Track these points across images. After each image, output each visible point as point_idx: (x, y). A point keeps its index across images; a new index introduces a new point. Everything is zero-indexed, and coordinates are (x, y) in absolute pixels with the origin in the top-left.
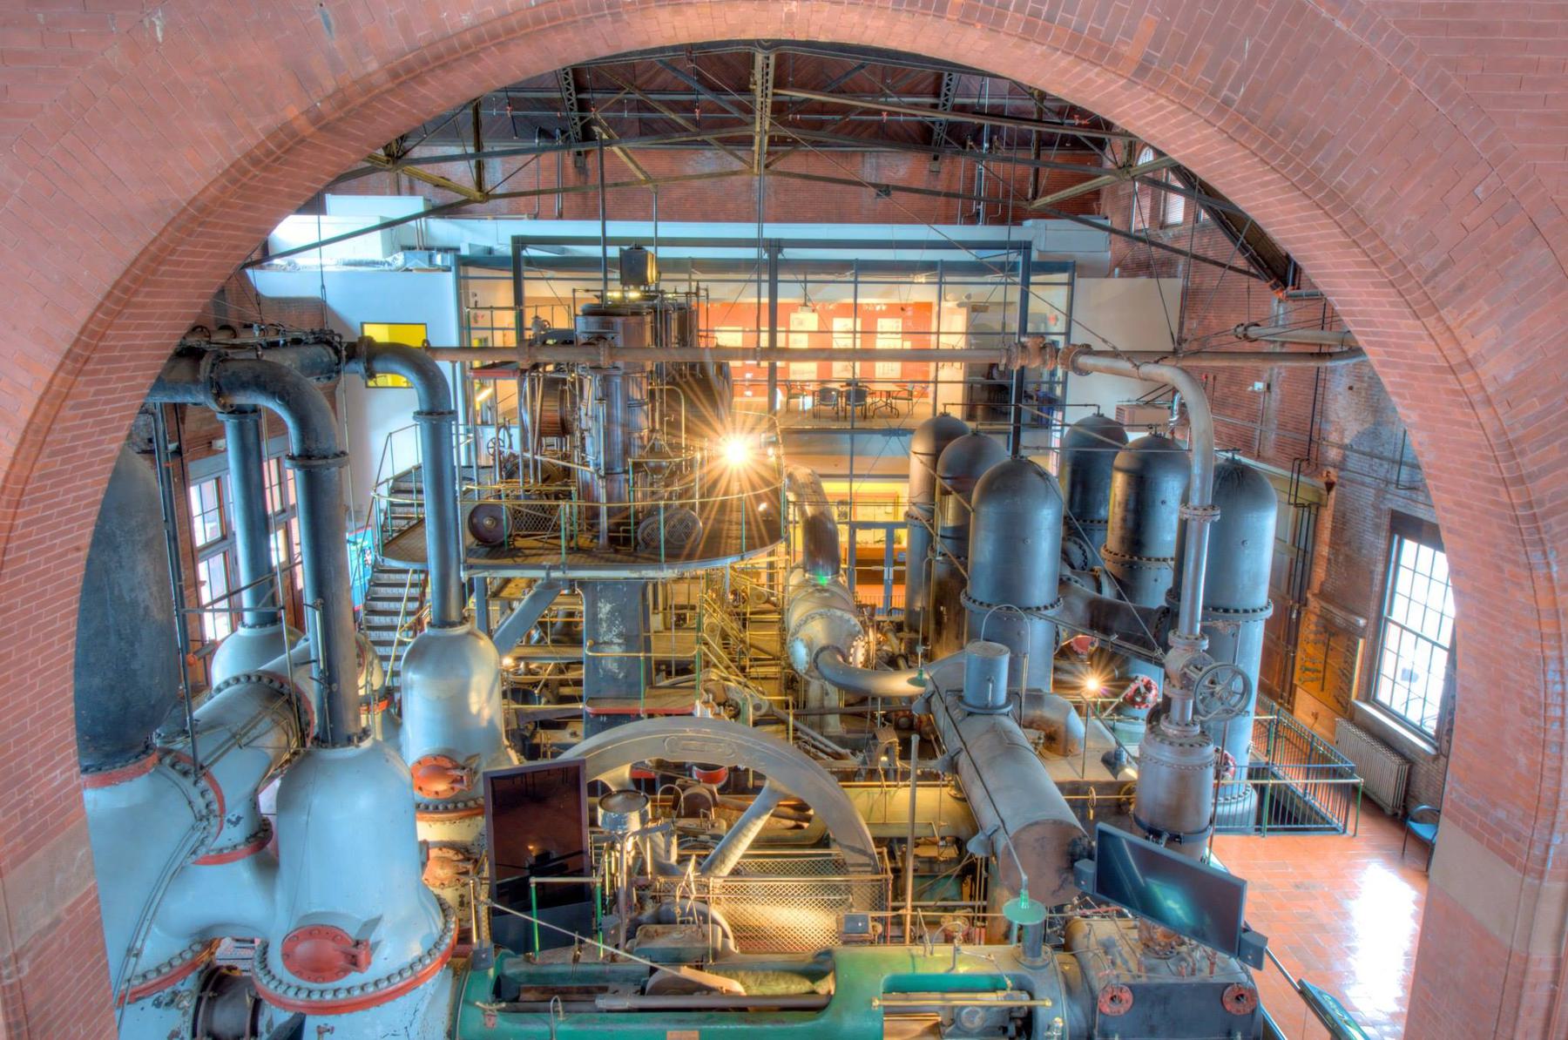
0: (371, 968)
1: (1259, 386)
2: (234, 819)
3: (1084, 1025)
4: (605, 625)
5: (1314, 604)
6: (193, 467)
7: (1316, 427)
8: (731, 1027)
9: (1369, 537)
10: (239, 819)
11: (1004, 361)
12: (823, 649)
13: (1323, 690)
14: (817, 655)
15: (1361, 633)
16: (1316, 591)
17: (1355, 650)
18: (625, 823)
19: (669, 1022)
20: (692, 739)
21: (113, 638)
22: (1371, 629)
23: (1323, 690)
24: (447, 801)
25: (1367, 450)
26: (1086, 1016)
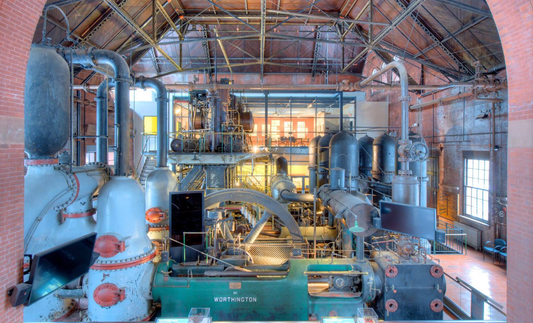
0: (124, 253)
1: (415, 125)
2: (83, 203)
3: (381, 283)
4: (213, 181)
5: (441, 188)
6: (87, 147)
7: (435, 132)
8: (253, 281)
9: (456, 161)
10: (85, 203)
11: (338, 88)
12: (283, 190)
13: (447, 215)
14: (281, 193)
15: (458, 192)
16: (441, 183)
17: (457, 199)
18: (217, 216)
19: (230, 280)
20: (240, 193)
21: (47, 110)
22: (461, 190)
23: (447, 215)
24: (157, 224)
25: (452, 134)
26: (381, 279)
